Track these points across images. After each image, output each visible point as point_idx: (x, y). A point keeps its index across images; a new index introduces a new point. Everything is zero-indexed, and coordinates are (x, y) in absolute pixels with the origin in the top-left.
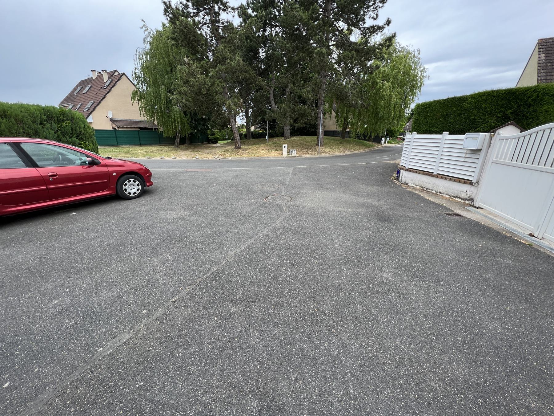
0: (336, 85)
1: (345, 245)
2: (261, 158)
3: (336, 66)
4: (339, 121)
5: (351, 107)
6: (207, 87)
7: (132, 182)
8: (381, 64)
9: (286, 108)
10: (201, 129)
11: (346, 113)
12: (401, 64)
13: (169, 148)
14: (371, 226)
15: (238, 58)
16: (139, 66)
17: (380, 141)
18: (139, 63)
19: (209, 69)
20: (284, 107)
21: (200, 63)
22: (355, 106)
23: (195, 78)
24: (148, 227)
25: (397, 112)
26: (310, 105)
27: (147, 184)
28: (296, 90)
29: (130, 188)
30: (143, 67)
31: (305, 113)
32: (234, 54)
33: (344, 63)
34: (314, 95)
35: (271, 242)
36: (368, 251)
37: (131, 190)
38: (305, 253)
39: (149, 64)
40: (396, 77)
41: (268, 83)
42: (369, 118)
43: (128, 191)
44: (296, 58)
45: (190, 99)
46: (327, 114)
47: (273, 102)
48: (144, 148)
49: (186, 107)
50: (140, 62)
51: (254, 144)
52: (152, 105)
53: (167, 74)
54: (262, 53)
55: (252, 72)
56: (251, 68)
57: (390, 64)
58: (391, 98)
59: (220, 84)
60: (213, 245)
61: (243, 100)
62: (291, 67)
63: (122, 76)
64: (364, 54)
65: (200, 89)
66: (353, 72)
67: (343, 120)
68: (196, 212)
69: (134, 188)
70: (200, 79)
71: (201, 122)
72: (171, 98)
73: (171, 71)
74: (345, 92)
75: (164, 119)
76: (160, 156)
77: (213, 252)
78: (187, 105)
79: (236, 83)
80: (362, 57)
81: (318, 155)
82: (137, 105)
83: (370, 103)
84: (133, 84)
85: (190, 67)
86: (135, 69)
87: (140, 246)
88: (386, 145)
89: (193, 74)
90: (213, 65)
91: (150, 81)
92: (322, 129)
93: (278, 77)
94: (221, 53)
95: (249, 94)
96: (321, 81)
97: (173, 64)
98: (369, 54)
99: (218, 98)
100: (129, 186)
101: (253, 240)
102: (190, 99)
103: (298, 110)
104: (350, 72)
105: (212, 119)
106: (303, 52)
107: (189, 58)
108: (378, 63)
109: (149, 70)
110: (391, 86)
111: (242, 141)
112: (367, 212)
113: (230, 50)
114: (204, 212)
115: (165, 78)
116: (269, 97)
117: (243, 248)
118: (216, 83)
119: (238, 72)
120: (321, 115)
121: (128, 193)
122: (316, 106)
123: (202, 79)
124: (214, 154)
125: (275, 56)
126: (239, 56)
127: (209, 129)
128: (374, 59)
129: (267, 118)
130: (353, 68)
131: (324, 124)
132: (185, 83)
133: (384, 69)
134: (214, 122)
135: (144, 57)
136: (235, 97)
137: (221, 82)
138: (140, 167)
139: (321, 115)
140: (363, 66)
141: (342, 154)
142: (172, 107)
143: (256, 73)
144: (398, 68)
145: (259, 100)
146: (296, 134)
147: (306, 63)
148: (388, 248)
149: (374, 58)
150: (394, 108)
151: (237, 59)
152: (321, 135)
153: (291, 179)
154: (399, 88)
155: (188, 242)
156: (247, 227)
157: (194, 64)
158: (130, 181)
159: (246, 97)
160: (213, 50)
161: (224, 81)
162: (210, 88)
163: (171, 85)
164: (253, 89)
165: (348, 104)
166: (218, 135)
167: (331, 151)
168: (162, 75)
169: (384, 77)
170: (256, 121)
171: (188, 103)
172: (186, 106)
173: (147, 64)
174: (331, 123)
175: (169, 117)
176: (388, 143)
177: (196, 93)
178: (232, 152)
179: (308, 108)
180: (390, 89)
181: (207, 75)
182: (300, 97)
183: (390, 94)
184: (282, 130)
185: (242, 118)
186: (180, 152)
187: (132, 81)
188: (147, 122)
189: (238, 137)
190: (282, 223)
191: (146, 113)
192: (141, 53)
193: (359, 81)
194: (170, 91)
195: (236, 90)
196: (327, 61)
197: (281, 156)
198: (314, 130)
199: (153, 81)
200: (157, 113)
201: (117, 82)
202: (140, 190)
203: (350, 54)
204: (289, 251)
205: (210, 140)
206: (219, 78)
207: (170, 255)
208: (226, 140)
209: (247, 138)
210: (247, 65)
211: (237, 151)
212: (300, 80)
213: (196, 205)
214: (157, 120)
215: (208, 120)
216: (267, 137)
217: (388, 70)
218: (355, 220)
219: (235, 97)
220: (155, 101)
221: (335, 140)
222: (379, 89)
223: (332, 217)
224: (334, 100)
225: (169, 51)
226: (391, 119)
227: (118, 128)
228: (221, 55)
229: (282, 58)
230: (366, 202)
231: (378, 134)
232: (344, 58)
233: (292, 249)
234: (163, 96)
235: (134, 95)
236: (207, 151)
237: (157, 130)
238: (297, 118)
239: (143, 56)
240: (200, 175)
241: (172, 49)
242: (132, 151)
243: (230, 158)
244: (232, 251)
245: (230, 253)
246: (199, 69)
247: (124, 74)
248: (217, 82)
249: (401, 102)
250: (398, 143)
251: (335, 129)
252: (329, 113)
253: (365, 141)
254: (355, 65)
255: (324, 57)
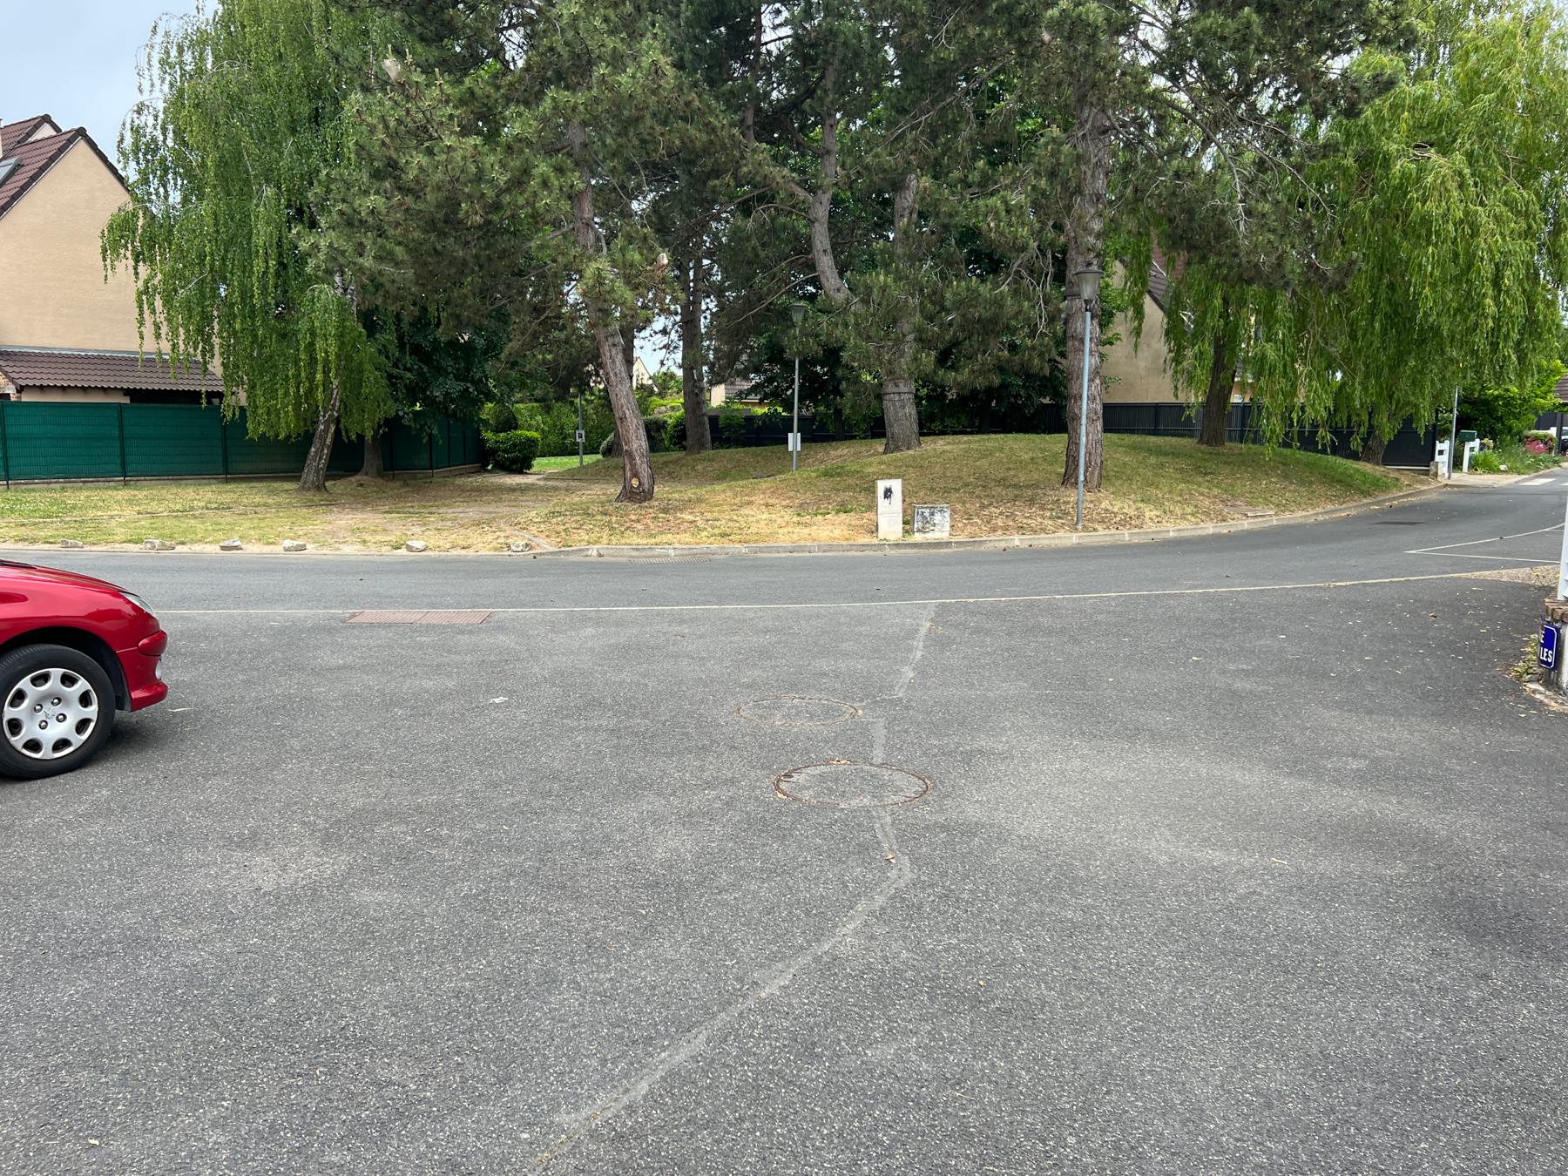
0: (1161, 172)
1: (1258, 1092)
2: (761, 550)
3: (1158, 82)
4: (1189, 353)
5: (1250, 282)
6: (490, 193)
7: (54, 683)
8: (1402, 64)
9: (898, 292)
10: (447, 394)
11: (1224, 315)
12: (1509, 62)
13: (273, 492)
14: (1412, 968)
15: (654, 52)
16: (158, 98)
17: (1425, 457)
18: (157, 82)
19: (506, 106)
20: (884, 288)
21: (460, 82)
22: (1273, 280)
23: (430, 152)
24: (109, 941)
25: (1515, 301)
26: (1024, 273)
27: (137, 694)
28: (949, 199)
29: (41, 716)
30: (177, 101)
31: (996, 315)
32: (634, 35)
33: (1204, 67)
34: (1044, 223)
35: (810, 1053)
36: (1404, 1134)
37: (44, 725)
38: (1011, 1135)
39: (209, 88)
40: (1488, 128)
41: (802, 171)
42: (1353, 337)
43: (29, 731)
44: (950, 52)
45: (399, 250)
46: (1119, 316)
47: (826, 264)
48: (140, 494)
49: (379, 286)
50: (163, 80)
51: (722, 477)
52: (203, 281)
53: (294, 131)
54: (775, 27)
55: (722, 120)
56: (717, 98)
57: (1452, 63)
58: (1475, 234)
59: (555, 182)
60: (470, 1067)
61: (673, 253)
62: (923, 91)
63: (70, 141)
64: (1309, 24)
65: (452, 203)
66: (1252, 107)
67: (1210, 350)
68: (386, 860)
69: (62, 718)
70: (458, 156)
71: (448, 363)
72: (304, 246)
73: (316, 118)
74: (1214, 208)
75: (261, 347)
76: (220, 535)
77: (467, 1112)
78: (382, 280)
79: (636, 173)
80: (1299, 37)
81: (1075, 535)
82: (126, 277)
83: (1352, 263)
84: (121, 179)
85: (408, 98)
86: (139, 111)
87: (55, 1060)
88: (1464, 477)
89: (422, 134)
90: (529, 90)
91: (203, 165)
92: (1092, 399)
93: (856, 140)
94: (570, 35)
95: (704, 226)
96: (1079, 159)
97: (327, 84)
98: (1331, 20)
99: (541, 247)
100: (38, 706)
101: (698, 1042)
102: (399, 250)
103: (959, 304)
104: (1235, 106)
105: (506, 351)
106: (984, 23)
107: (409, 58)
108: (1386, 60)
109: (205, 114)
110: (1467, 171)
111: (661, 457)
112: (1380, 879)
113: (613, 17)
114: (433, 860)
115: (281, 153)
116: (809, 239)
117: (643, 1087)
118: (535, 172)
119: (649, 121)
120: (1088, 327)
121: (26, 746)
122: (1060, 278)
123: (464, 158)
124: (509, 530)
125: (841, 39)
126: (657, 44)
127: (489, 396)
128: (1363, 43)
129: (795, 343)
130: (1247, 89)
131: (1103, 372)
132: (377, 175)
133: (1420, 91)
134: (514, 364)
135: (188, 57)
136: (630, 239)
137: (560, 170)
138: (107, 602)
139: (1088, 327)
140: (1306, 80)
141: (1210, 528)
142: (302, 291)
143: (742, 121)
144: (1494, 82)
145: (757, 256)
146: (948, 422)
147: (998, 72)
148: (1529, 1120)
149: (1362, 37)
150: (1497, 282)
151: (646, 62)
152: (1088, 429)
153: (921, 672)
154: (1512, 181)
155: (326, 1040)
156: (670, 954)
157: (428, 86)
158: (45, 678)
159: (689, 238)
160: (529, 21)
161: (577, 164)
162: (507, 198)
163: (311, 184)
164: (722, 199)
165: (1230, 268)
166: (532, 423)
167: (1150, 512)
168: (268, 136)
169: (1421, 127)
170: (735, 357)
171: (387, 268)
172: (375, 283)
173: (200, 89)
174: (1141, 363)
175: (283, 336)
176: (1474, 466)
177: (432, 222)
178: (607, 518)
179: (1015, 292)
180: (1461, 186)
181: (492, 137)
182: (970, 235)
183: (1466, 213)
184: (874, 402)
185: (665, 340)
186: (329, 518)
187: (119, 167)
188: (179, 364)
189: (637, 442)
190: (872, 937)
191: (169, 320)
192: (176, 38)
193: (1286, 154)
194: (300, 211)
195: (635, 205)
196: (1113, 58)
197: (866, 539)
198: (1046, 401)
199: (218, 166)
200: (229, 319)
201: (42, 169)
202: (92, 725)
203: (1232, 25)
204: (916, 1118)
205: (493, 452)
206: (551, 151)
207: (214, 1125)
208: (574, 453)
209: (689, 442)
210: (695, 85)
211: (633, 510)
212: (968, 151)
213: (388, 815)
214: (222, 354)
215: (485, 352)
216: (794, 440)
217: (1440, 92)
218: (1312, 927)
219: (630, 239)
220: (223, 259)
221: (1166, 454)
222: (1402, 189)
223: (1173, 902)
224: (1155, 245)
225: (310, 26)
226: (1480, 342)
227: (20, 390)
228: (567, 44)
229: (876, 48)
230: (1371, 813)
231: (1408, 421)
232: (1199, 43)
233: (933, 1104)
234: (262, 234)
235: (119, 234)
236: (473, 512)
237: (216, 401)
238: (956, 343)
239: (181, 51)
240: (422, 646)
241: (326, 19)
242: (74, 507)
243: (593, 551)
244: (577, 1109)
245: (561, 1118)
246: (456, 107)
247: (81, 133)
248: (542, 167)
249: (1531, 252)
250: (1534, 468)
251: (1166, 397)
252: (1130, 313)
253: (1340, 460)
254: (1262, 73)
255: (1093, 40)
